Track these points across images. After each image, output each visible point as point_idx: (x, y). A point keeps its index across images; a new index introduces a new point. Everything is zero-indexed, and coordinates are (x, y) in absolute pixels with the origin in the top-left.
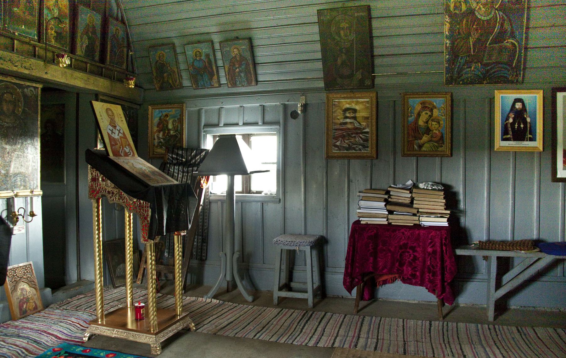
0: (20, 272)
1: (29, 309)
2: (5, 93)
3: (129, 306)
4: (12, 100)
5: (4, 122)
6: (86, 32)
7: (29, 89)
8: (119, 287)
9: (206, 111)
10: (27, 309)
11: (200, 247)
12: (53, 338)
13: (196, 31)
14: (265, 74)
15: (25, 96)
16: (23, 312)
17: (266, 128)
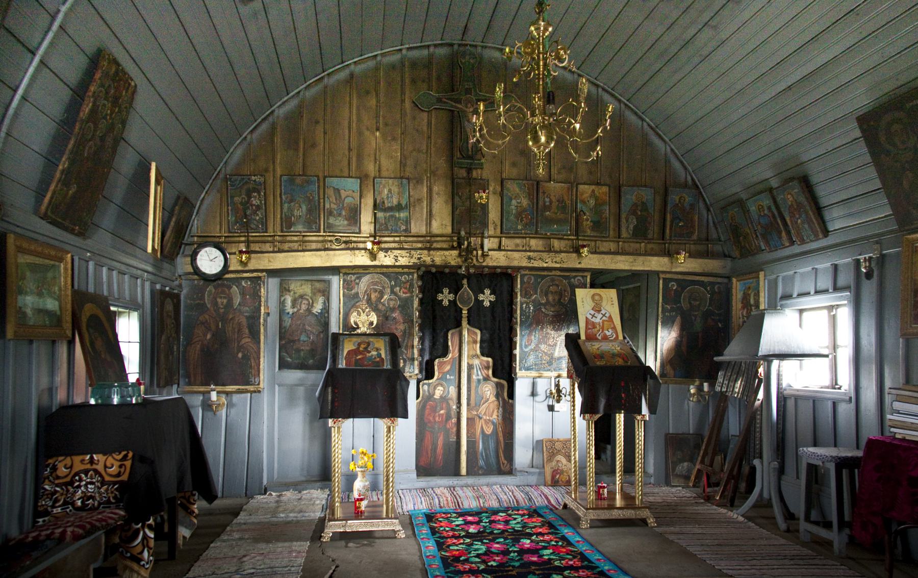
2: (551, 286)
3: (617, 491)
6: (633, 212)
7: (576, 279)
8: (676, 486)
9: (784, 278)
11: (757, 451)
12: (546, 501)
13: (755, 180)
14: (837, 220)
17: (837, 296)
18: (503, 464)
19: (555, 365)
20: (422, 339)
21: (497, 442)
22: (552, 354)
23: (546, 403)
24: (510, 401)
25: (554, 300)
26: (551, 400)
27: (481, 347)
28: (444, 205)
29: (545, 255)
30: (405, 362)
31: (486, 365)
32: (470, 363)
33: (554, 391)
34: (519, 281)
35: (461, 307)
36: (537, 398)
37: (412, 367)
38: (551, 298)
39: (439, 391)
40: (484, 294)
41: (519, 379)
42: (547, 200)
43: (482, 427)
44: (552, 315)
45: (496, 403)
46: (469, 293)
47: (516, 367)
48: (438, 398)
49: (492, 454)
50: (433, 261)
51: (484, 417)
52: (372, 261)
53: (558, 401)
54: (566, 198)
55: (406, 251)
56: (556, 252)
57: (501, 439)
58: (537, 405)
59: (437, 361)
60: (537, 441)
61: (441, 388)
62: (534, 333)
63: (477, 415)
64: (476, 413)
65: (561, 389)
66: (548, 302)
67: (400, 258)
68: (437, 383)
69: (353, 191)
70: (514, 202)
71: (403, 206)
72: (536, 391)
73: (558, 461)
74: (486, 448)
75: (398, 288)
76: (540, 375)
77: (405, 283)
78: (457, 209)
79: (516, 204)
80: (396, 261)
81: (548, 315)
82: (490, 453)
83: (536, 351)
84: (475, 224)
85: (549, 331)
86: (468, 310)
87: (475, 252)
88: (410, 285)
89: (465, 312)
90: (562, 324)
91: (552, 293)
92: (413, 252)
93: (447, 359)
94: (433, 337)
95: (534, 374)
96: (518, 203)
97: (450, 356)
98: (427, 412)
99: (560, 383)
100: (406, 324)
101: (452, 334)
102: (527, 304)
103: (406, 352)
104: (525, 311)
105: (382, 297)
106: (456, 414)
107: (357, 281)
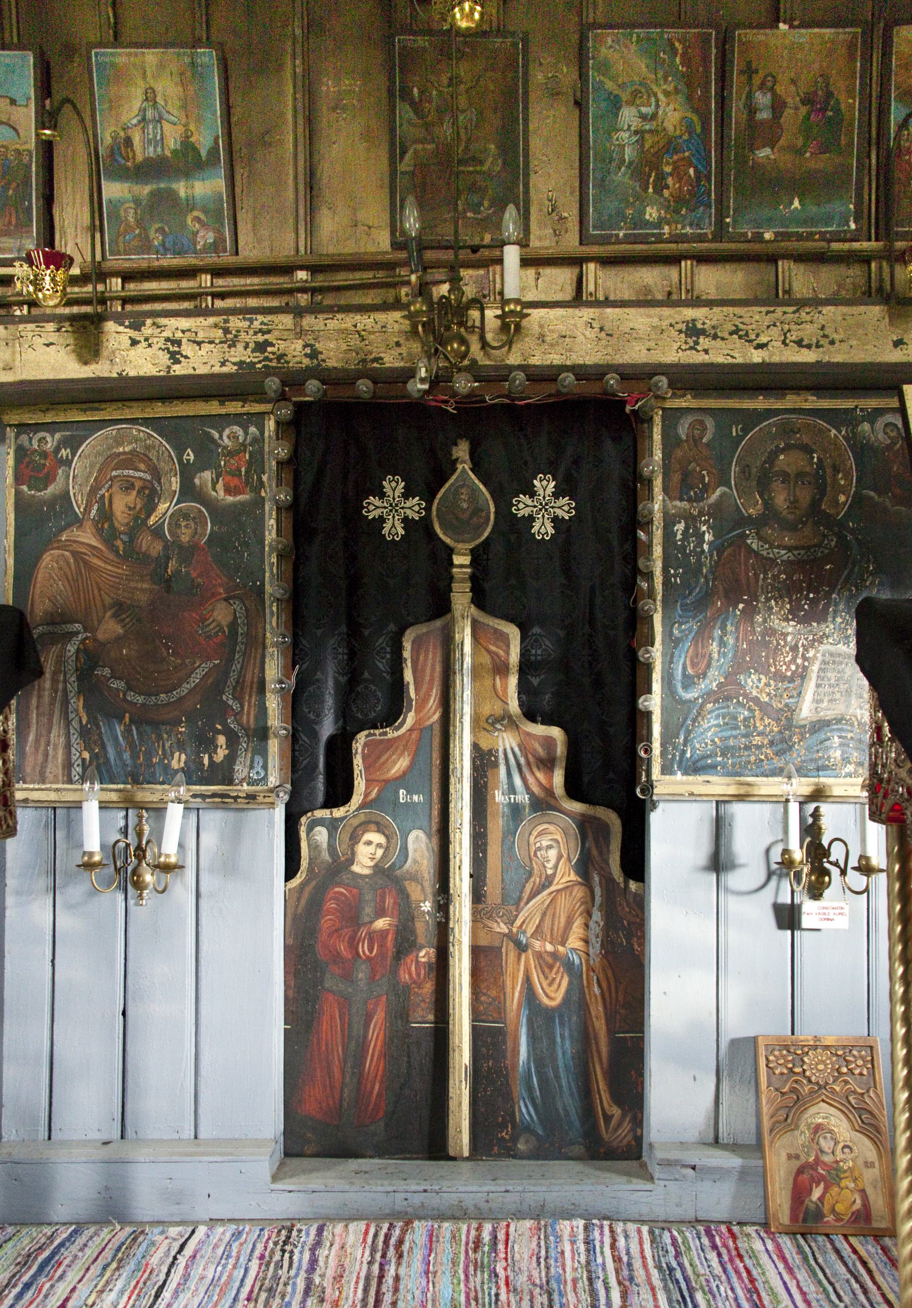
0: (821, 1067)
1: (833, 1211)
2: (783, 451)
4: (808, 469)
5: (778, 547)
7: (880, 423)
10: (826, 1209)
15: (862, 449)
16: (806, 1213)
18: (608, 1118)
19: (799, 752)
20: (434, 654)
21: (586, 1037)
22: (791, 710)
23: (767, 897)
24: (633, 886)
25: (794, 503)
26: (786, 886)
27: (523, 688)
28: (361, 146)
29: (755, 316)
30: (233, 741)
31: (541, 751)
32: (485, 745)
33: (798, 855)
34: (657, 436)
35: (448, 541)
36: (734, 879)
37: (258, 759)
38: (781, 499)
39: (371, 849)
40: (532, 494)
41: (661, 806)
42: (762, 99)
43: (528, 979)
44: (790, 562)
45: (579, 892)
46: (474, 491)
47: (649, 761)
48: (367, 872)
49: (566, 1082)
50: (314, 355)
51: (537, 944)
52: (86, 363)
53: (816, 892)
54: (839, 86)
55: (211, 320)
56: (801, 303)
57: (600, 1025)
58: (733, 904)
59: (362, 737)
60: (734, 1043)
61: (377, 838)
62: (717, 632)
63: (510, 936)
64: (504, 929)
65: (825, 842)
66: (769, 515)
67: (187, 349)
68: (362, 818)
69: (13, 102)
70: (628, 116)
71: (204, 153)
72: (730, 853)
73: (818, 1128)
74: (540, 1059)
75: (207, 475)
76: (742, 791)
77: (231, 454)
78: (404, 152)
79: (636, 123)
80: (175, 358)
81: (773, 561)
82: (557, 1077)
83: (728, 698)
84: (476, 208)
85: (776, 623)
86: (475, 554)
87: (475, 314)
88: (250, 463)
89: (461, 560)
90: (828, 596)
91: (785, 477)
92: (236, 323)
93: (396, 734)
94: (352, 654)
95: (720, 785)
96: (643, 117)
97: (410, 719)
98: (327, 922)
99: (824, 822)
100: (237, 606)
101: (418, 644)
102: (691, 520)
103: (236, 706)
104: (684, 547)
105: (150, 508)
106: (432, 927)
107: (64, 453)
